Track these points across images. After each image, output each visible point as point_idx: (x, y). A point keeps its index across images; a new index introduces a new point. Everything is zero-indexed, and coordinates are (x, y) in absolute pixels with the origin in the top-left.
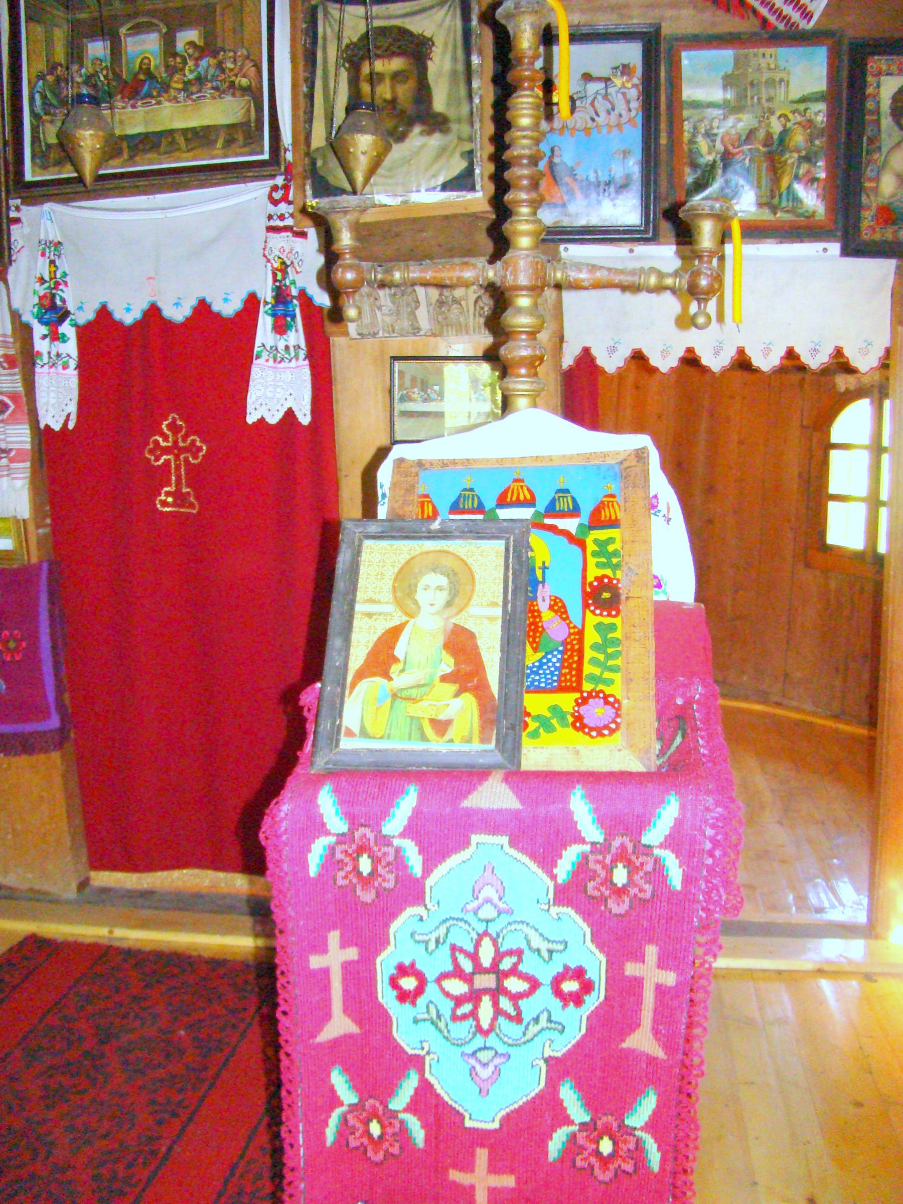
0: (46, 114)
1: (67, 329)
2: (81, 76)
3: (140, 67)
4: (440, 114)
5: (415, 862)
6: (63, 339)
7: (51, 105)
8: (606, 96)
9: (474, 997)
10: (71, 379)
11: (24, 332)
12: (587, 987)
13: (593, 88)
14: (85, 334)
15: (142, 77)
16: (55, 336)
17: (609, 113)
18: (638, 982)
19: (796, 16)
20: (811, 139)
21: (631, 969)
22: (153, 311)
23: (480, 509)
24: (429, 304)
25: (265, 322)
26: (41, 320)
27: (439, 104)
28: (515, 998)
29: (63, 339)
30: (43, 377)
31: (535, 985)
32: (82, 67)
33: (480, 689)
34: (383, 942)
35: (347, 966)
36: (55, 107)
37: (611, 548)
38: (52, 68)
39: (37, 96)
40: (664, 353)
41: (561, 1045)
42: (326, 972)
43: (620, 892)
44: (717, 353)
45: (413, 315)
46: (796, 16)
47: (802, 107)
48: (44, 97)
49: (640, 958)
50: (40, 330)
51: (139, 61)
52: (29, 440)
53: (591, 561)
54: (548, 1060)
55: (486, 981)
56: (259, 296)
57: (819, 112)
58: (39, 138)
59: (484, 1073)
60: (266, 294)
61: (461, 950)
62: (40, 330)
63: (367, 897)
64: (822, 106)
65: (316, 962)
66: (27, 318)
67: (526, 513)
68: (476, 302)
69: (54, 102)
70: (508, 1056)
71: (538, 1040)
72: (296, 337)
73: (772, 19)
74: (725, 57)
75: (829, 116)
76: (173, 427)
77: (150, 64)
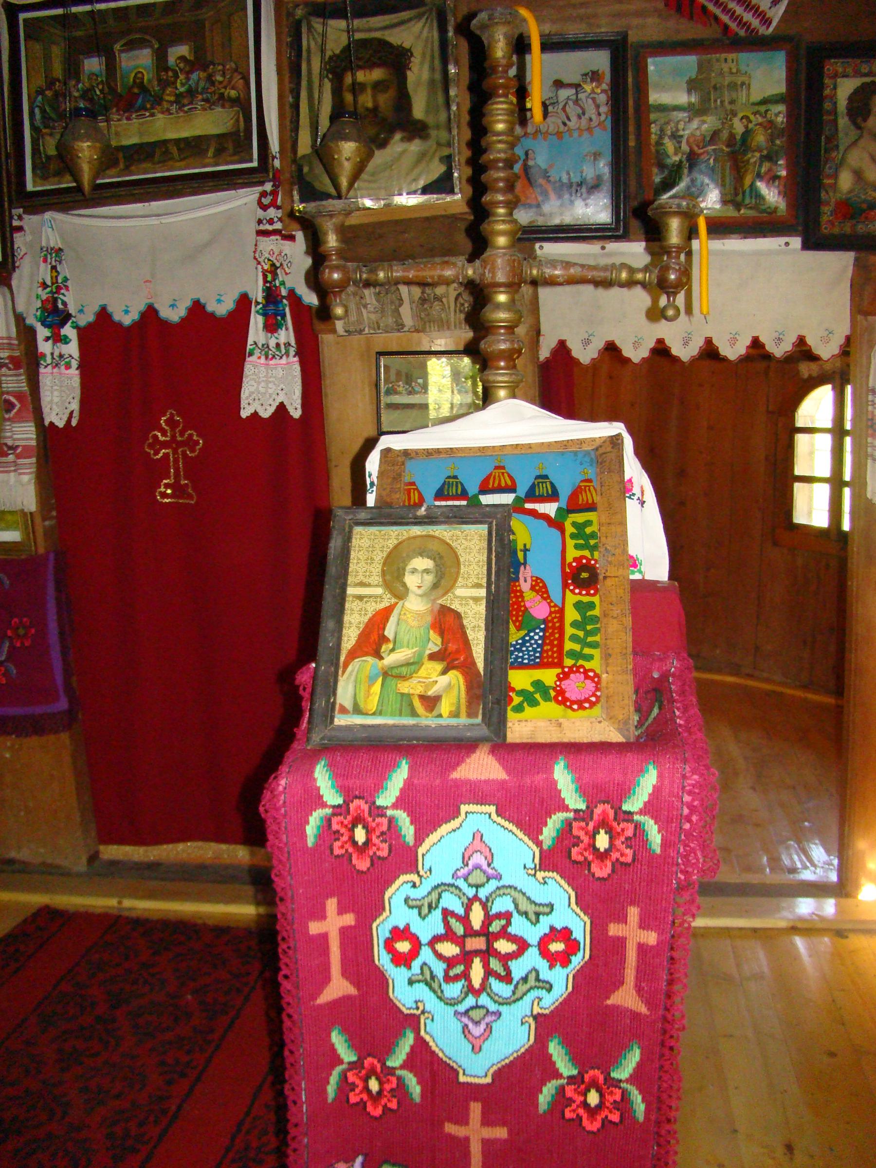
0: (45, 127)
1: (68, 331)
2: (78, 90)
3: (134, 81)
4: (419, 121)
5: (408, 830)
6: (66, 340)
7: (50, 118)
8: (576, 102)
9: (466, 958)
10: (73, 376)
11: (27, 334)
12: (573, 947)
13: (564, 93)
14: (84, 334)
15: (136, 91)
16: (57, 338)
17: (579, 117)
18: (621, 942)
19: (755, 23)
20: (772, 139)
21: (614, 930)
22: (150, 313)
23: (464, 495)
24: (412, 302)
25: (256, 322)
26: (44, 324)
27: (419, 111)
28: (505, 958)
29: (66, 340)
30: (47, 377)
31: (523, 945)
32: (78, 82)
33: (467, 667)
34: (377, 907)
35: (344, 932)
36: (53, 120)
37: (588, 530)
38: (51, 83)
39: (37, 111)
40: (636, 345)
41: (549, 1001)
42: (324, 937)
43: (602, 856)
44: (686, 343)
45: (397, 313)
46: (755, 23)
47: (763, 109)
48: (43, 111)
49: (623, 919)
50: (42, 332)
51: (133, 75)
52: (35, 437)
53: (570, 543)
54: (537, 1017)
55: (476, 943)
56: (250, 296)
57: (779, 113)
58: (39, 150)
59: (477, 1031)
60: (258, 294)
61: (453, 914)
62: (42, 332)
63: (363, 864)
64: (782, 108)
65: (315, 928)
66: (31, 321)
67: (507, 499)
68: (456, 299)
69: (53, 116)
70: (498, 1014)
71: (528, 998)
72: (286, 335)
73: (733, 26)
74: (690, 61)
75: (789, 115)
76: (171, 422)
77: (143, 79)
